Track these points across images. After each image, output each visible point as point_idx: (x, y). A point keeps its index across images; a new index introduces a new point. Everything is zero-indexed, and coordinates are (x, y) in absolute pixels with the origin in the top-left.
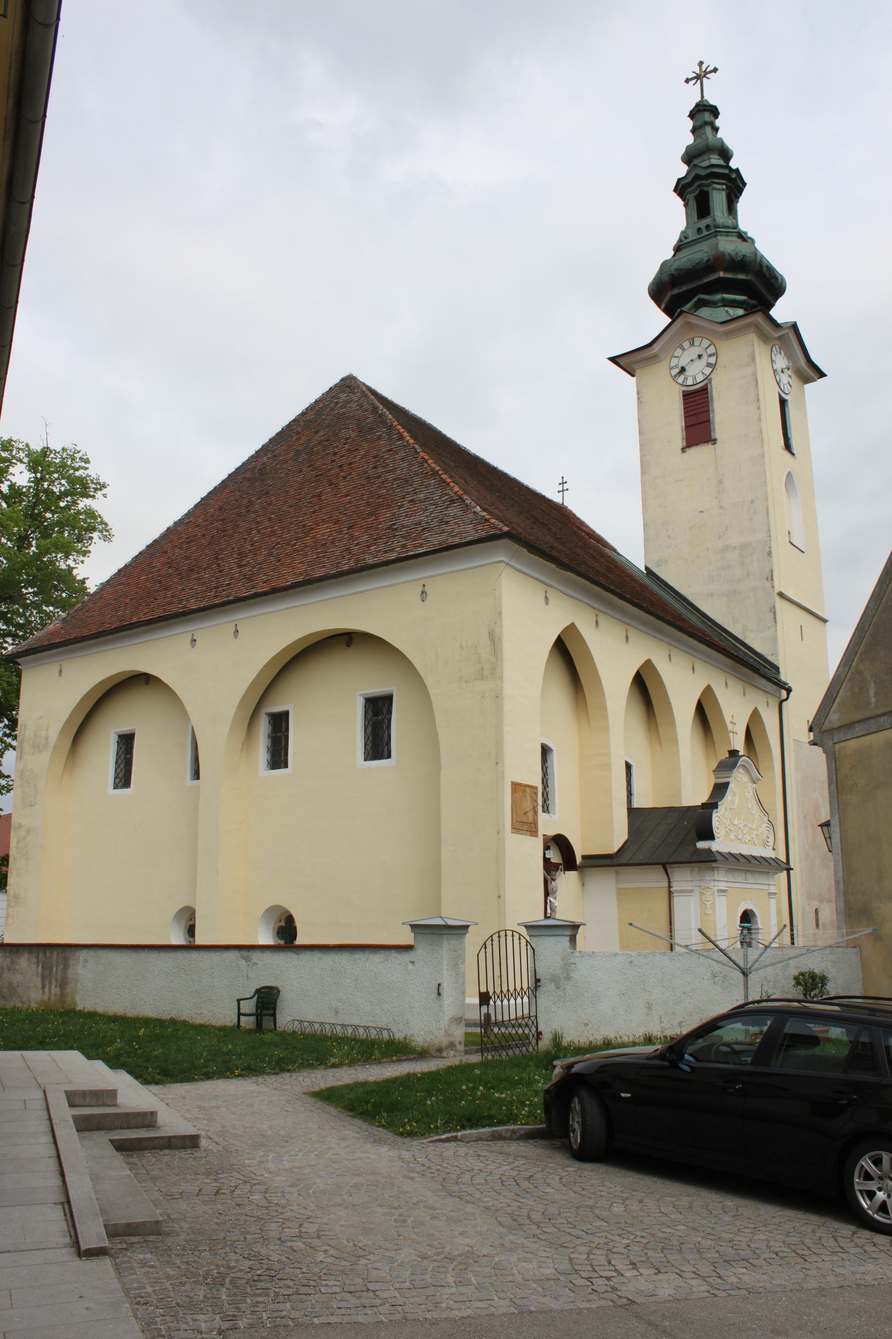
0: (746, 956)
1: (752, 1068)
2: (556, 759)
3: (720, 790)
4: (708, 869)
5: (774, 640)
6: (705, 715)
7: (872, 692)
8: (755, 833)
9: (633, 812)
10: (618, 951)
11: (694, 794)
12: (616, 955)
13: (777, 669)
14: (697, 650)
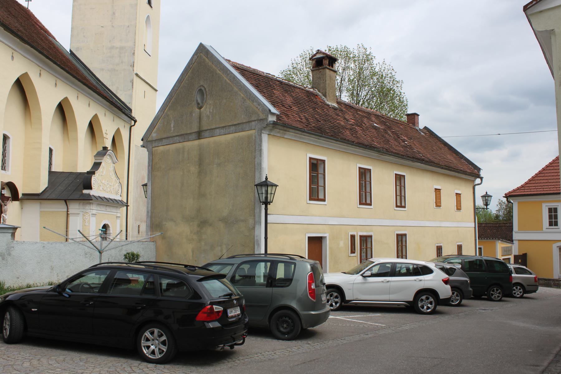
0: (101, 244)
1: (98, 294)
2: (11, 143)
3: (97, 165)
4: (88, 203)
5: (131, 96)
6: (93, 128)
7: (172, 125)
8: (112, 187)
9: (51, 173)
10: (38, 240)
11: (84, 167)
12: (36, 243)
13: (131, 110)
14: (92, 96)
